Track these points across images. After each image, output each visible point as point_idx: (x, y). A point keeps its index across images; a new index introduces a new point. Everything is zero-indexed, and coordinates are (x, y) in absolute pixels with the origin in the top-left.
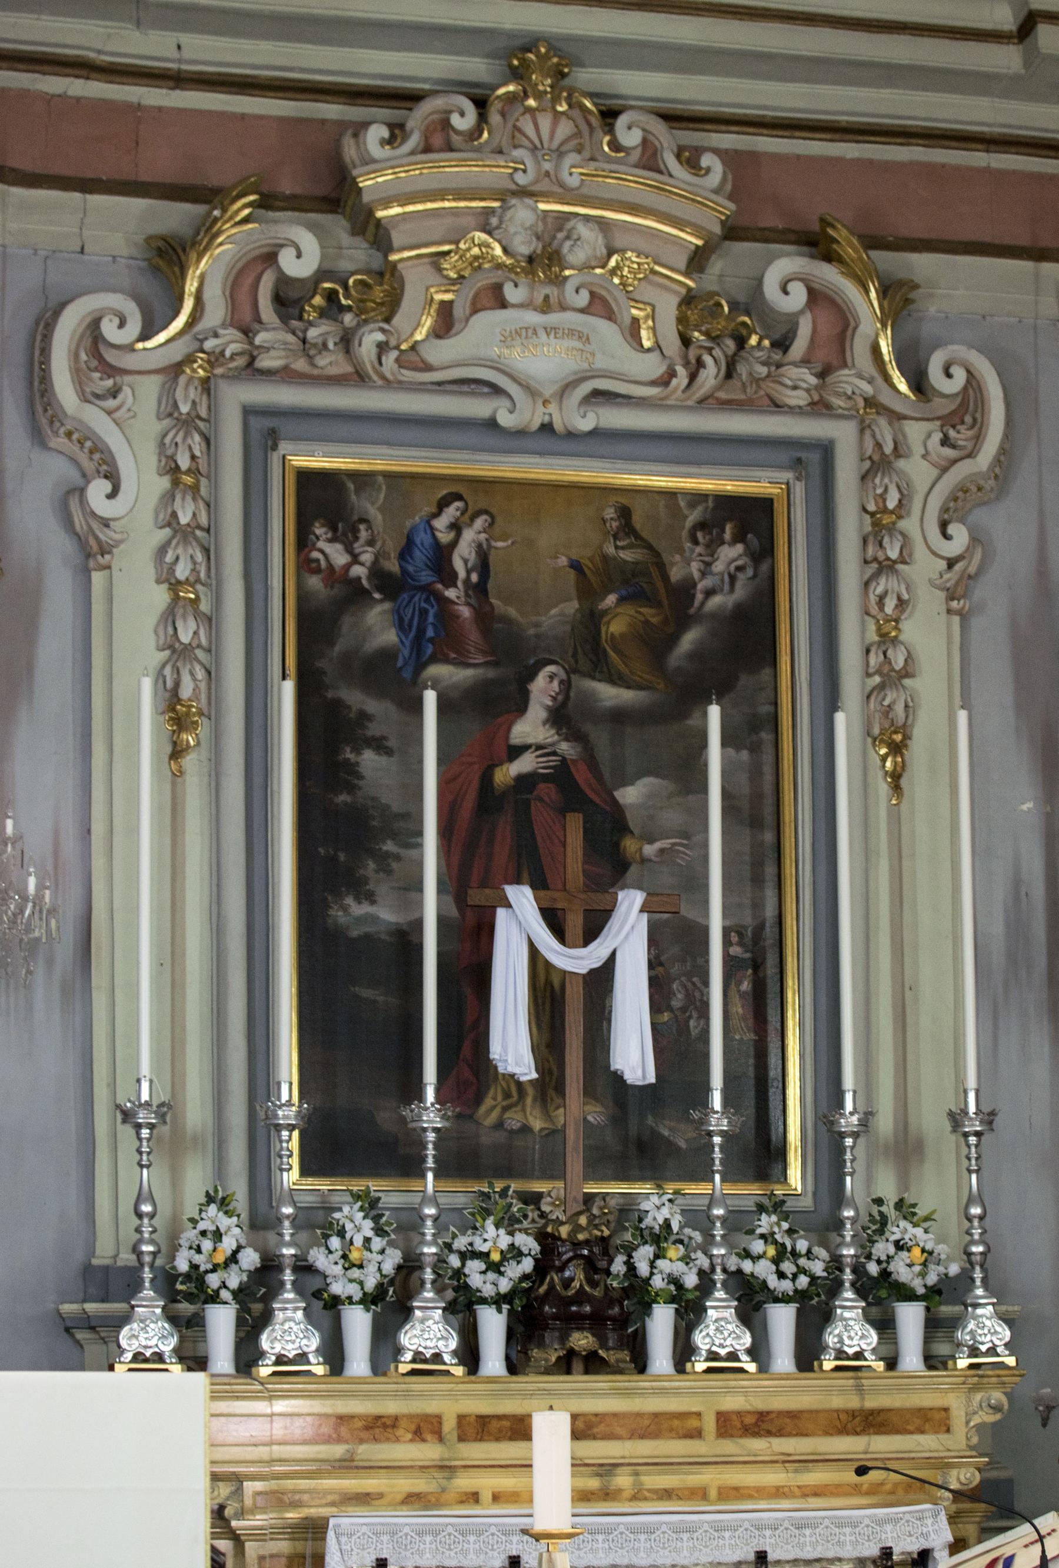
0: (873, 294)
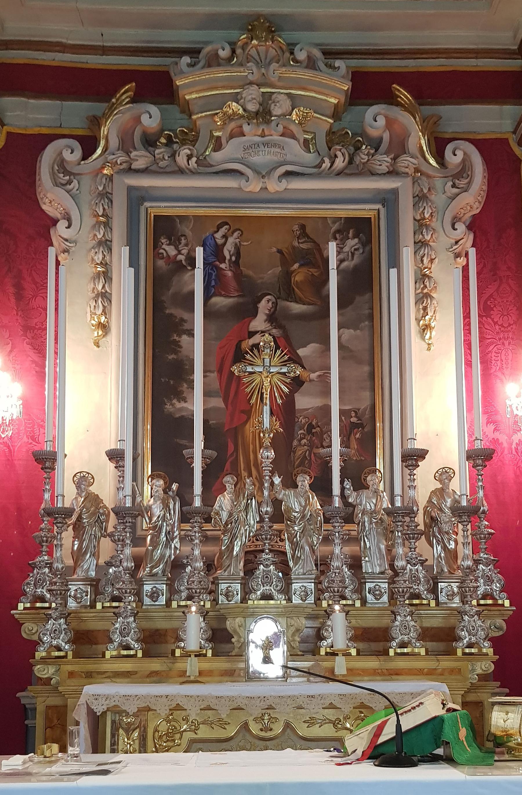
0: (418, 119)
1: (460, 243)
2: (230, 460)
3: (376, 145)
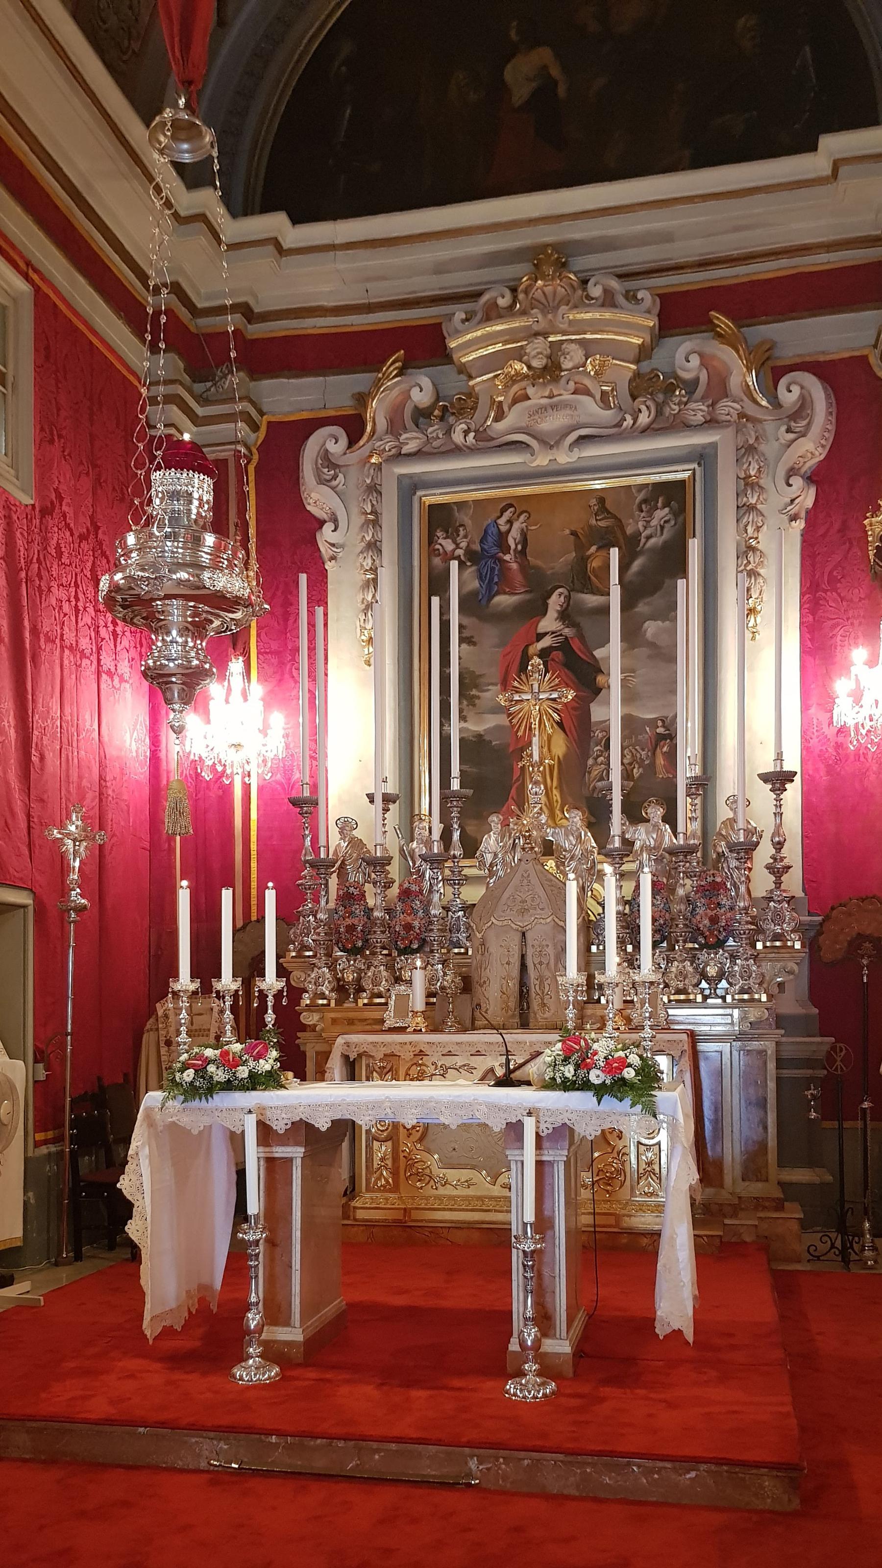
1: (796, 501)
2: (515, 785)
3: (691, 386)
